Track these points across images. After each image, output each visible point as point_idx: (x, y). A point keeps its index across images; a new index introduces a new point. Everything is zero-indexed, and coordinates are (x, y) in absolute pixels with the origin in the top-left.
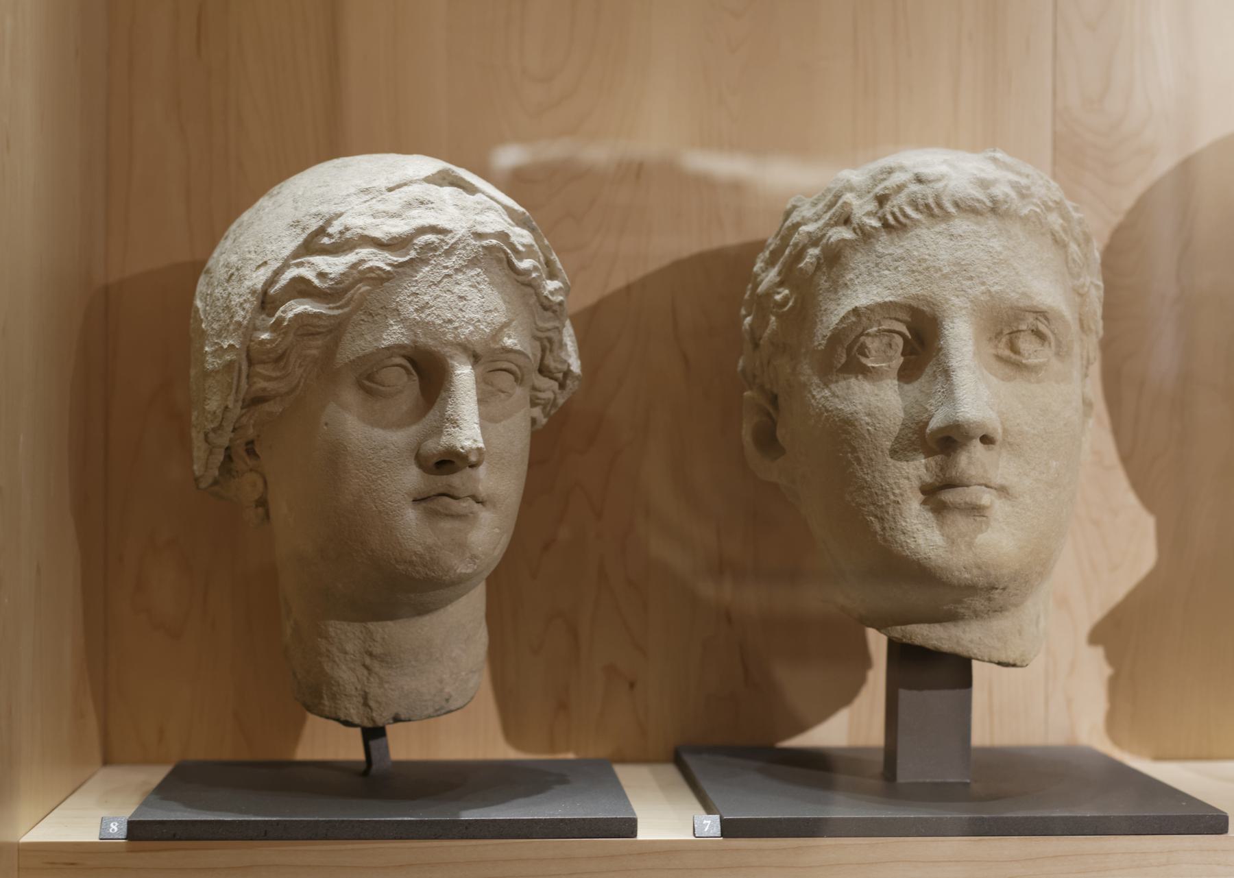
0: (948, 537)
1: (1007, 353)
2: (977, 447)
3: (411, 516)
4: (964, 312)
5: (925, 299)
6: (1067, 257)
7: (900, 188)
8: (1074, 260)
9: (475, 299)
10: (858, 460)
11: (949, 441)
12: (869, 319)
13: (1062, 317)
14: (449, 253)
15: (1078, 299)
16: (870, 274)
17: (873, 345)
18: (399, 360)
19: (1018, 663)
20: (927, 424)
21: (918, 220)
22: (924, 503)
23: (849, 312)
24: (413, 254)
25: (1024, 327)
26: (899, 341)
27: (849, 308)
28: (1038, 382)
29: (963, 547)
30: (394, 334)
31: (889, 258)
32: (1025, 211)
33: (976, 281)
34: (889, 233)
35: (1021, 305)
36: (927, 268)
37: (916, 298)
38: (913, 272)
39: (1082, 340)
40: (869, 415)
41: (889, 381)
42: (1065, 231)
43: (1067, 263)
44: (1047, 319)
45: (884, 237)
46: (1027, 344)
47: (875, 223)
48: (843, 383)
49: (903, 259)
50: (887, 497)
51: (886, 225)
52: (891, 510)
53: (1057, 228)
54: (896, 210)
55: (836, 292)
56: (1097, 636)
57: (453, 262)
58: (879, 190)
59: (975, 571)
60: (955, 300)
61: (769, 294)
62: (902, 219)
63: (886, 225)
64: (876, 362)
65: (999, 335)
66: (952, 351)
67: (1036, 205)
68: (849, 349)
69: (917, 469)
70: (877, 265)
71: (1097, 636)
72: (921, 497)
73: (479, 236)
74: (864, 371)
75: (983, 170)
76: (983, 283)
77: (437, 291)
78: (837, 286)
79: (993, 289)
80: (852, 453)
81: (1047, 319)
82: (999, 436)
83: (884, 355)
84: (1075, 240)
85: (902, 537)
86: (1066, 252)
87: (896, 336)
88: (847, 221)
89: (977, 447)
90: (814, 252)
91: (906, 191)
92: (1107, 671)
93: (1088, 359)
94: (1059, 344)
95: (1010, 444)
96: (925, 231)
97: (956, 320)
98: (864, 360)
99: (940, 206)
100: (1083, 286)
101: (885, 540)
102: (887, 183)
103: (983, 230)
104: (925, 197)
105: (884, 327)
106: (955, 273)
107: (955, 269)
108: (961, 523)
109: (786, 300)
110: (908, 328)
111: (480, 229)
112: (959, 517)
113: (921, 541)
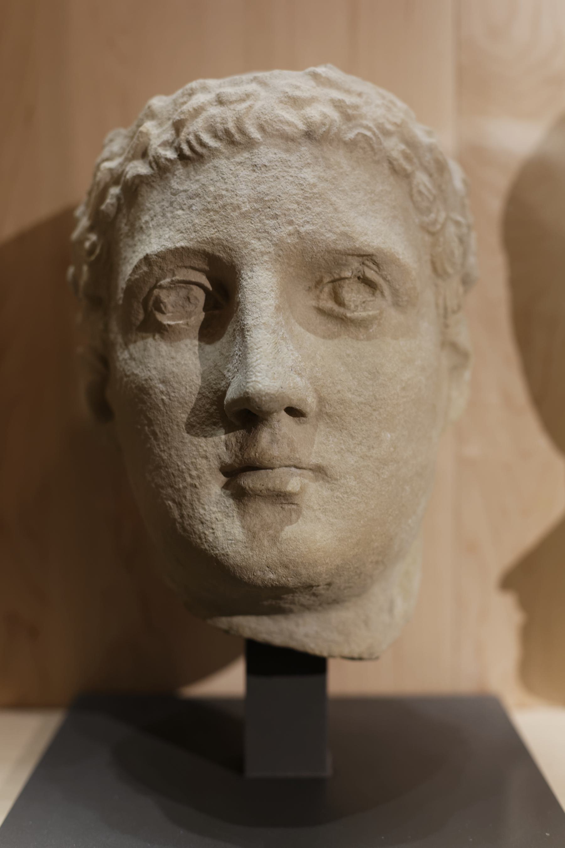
0: (249, 530)
1: (330, 305)
2: (284, 423)
4: (266, 258)
5: (220, 243)
6: (411, 189)
7: (198, 111)
8: (420, 193)
10: (154, 434)
11: (245, 416)
12: (161, 268)
13: (394, 261)
15: (427, 238)
16: (164, 215)
17: (169, 299)
19: (365, 656)
20: (224, 393)
21: (216, 149)
22: (226, 487)
23: (141, 261)
25: (348, 274)
26: (200, 295)
27: (141, 256)
28: (369, 338)
29: (266, 543)
31: (183, 195)
32: (351, 135)
33: (282, 220)
34: (185, 165)
35: (339, 247)
36: (224, 207)
37: (211, 242)
38: (208, 210)
39: (436, 286)
40: (163, 382)
41: (188, 341)
42: (407, 157)
43: (411, 196)
44: (375, 263)
45: (180, 170)
46: (353, 295)
47: (171, 154)
48: (140, 344)
49: (198, 195)
50: (184, 480)
51: (182, 157)
52: (188, 494)
53: (395, 154)
54: (191, 138)
55: (133, 238)
56: (511, 581)
58: (176, 117)
59: (281, 571)
60: (255, 244)
61: (81, 241)
62: (198, 148)
63: (182, 157)
64: (169, 319)
65: (319, 283)
66: (249, 306)
67: (369, 129)
68: (145, 304)
69: (215, 447)
70: (171, 204)
71: (511, 581)
72: (223, 479)
74: (161, 330)
75: (297, 87)
76: (291, 223)
78: (135, 229)
79: (302, 230)
80: (149, 427)
81: (375, 263)
82: (310, 403)
83: (183, 311)
84: (426, 170)
85: (200, 527)
86: (410, 184)
87: (194, 287)
88: (144, 155)
89: (284, 423)
90: (115, 191)
91: (204, 115)
93: (446, 309)
94: (395, 293)
95: (329, 416)
96: (223, 161)
97: (256, 268)
98: (159, 317)
99: (242, 131)
100: (435, 222)
101: (185, 530)
102: (185, 108)
103: (293, 158)
104: (224, 121)
105: (178, 278)
106: (257, 210)
107: (256, 206)
108: (268, 512)
109: (94, 245)
110: (209, 278)
112: (262, 505)
113: (219, 534)
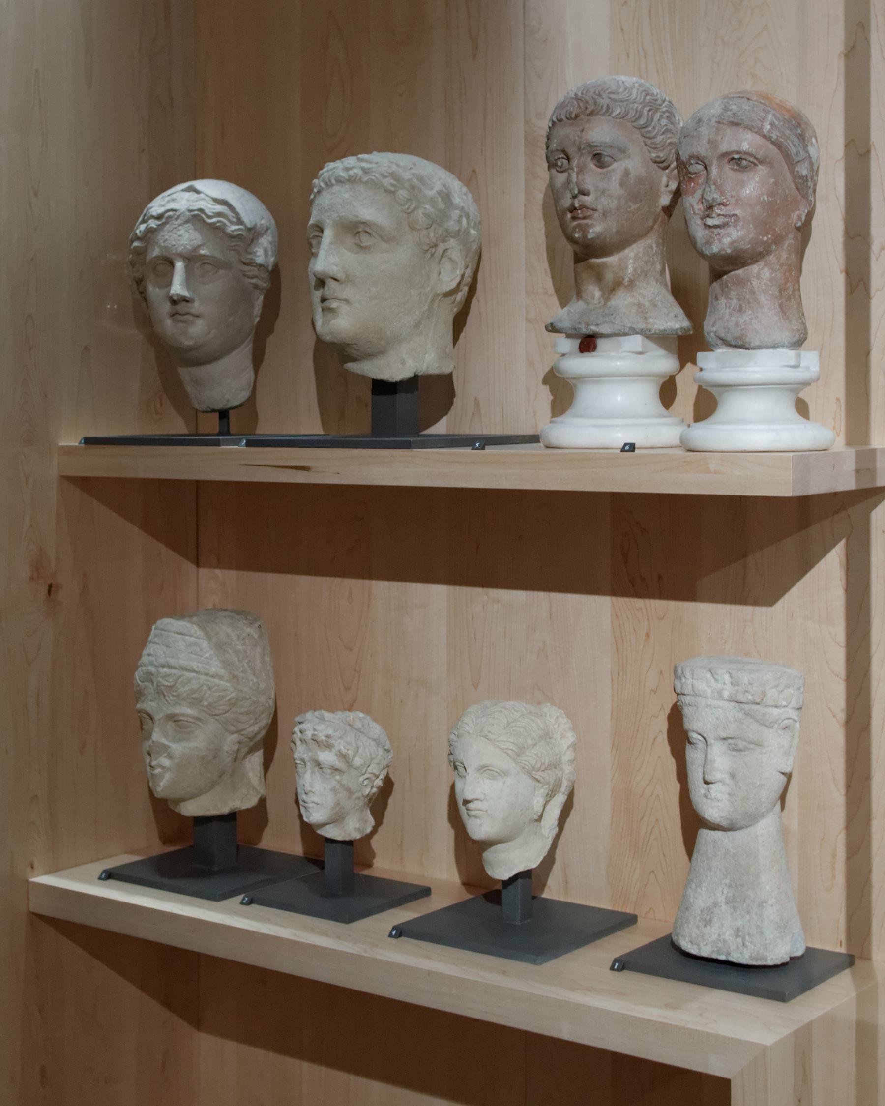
3: (169, 322)
9: (186, 236)
14: (177, 219)
18: (161, 262)
24: (164, 220)
30: (156, 252)
57: (179, 222)
73: (191, 211)
77: (170, 234)
92: (551, 398)
111: (191, 208)
